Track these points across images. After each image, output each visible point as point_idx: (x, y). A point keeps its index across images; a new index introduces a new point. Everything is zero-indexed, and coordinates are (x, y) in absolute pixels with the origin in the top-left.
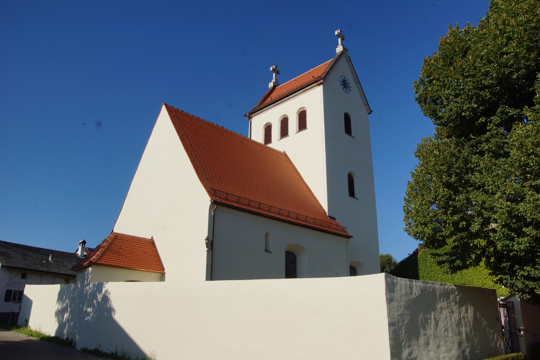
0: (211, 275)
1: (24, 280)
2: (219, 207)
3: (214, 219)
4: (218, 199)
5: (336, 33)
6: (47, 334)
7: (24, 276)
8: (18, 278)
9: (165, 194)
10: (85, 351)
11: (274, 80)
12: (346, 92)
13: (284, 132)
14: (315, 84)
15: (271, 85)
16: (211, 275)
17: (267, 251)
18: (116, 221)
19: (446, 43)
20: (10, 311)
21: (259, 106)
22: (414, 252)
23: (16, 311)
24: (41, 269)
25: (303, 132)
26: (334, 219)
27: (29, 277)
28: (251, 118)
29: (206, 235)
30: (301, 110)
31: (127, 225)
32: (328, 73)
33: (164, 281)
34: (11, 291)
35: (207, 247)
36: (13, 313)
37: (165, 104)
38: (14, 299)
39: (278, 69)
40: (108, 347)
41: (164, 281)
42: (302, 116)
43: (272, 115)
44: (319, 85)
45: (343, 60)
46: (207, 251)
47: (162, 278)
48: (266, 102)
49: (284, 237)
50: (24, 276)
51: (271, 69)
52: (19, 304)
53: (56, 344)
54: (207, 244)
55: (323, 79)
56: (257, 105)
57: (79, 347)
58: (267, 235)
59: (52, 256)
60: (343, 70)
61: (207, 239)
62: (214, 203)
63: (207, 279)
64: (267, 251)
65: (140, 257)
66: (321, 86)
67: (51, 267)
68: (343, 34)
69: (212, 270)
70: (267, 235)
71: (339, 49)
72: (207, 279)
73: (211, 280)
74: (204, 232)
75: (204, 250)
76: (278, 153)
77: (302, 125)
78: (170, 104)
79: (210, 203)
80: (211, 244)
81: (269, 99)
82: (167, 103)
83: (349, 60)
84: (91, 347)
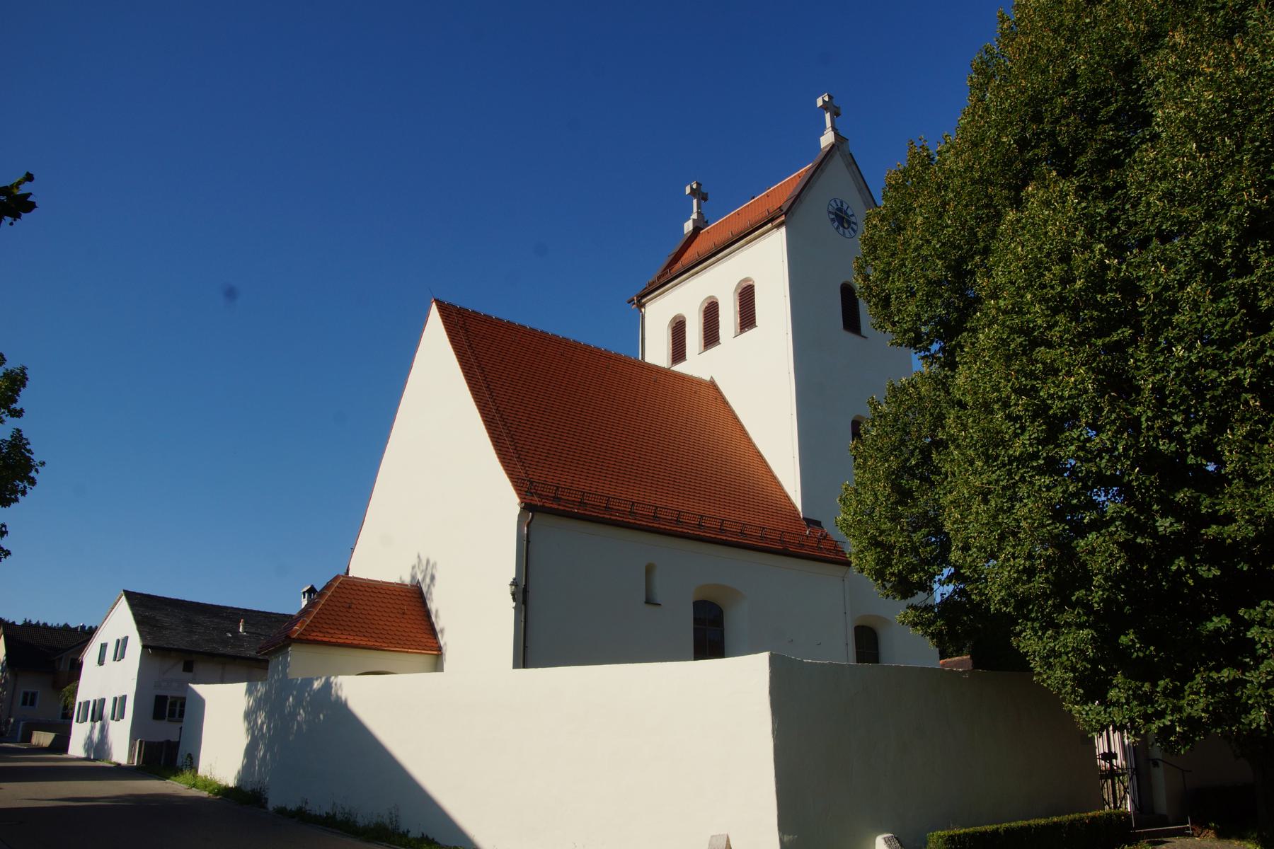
0: (525, 656)
1: (189, 675)
2: (538, 517)
3: (528, 542)
4: (536, 501)
5: (820, 103)
6: (224, 783)
7: (188, 667)
8: (177, 671)
9: (440, 495)
10: (282, 812)
11: (694, 216)
12: (844, 235)
13: (711, 337)
14: (770, 225)
15: (688, 227)
16: (525, 656)
17: (649, 601)
18: (353, 549)
19: (890, 186)
20: (162, 740)
21: (659, 278)
22: (439, 649)
23: (174, 738)
24: (222, 650)
25: (714, 350)
26: (818, 523)
27: (199, 668)
28: (643, 305)
29: (511, 573)
30: (744, 285)
31: (377, 559)
32: (797, 199)
33: (442, 670)
34: (166, 697)
35: (514, 599)
36: (168, 742)
37: (437, 301)
38: (172, 714)
39: (703, 190)
40: (368, 810)
41: (442, 670)
42: (746, 296)
43: (684, 299)
44: (779, 226)
45: (838, 162)
46: (515, 608)
47: (437, 666)
48: (675, 269)
49: (689, 571)
50: (188, 667)
51: (688, 190)
52: (178, 725)
53: (241, 800)
54: (513, 594)
55: (786, 214)
56: (659, 272)
57: (273, 802)
58: (649, 570)
59: (245, 623)
60: (838, 185)
61: (515, 583)
62: (527, 507)
63: (516, 666)
64: (649, 601)
65: (398, 622)
66: (783, 230)
67: (242, 646)
68: (835, 102)
69: (525, 647)
70: (649, 570)
71: (827, 139)
72: (516, 666)
73: (524, 667)
74: (507, 568)
75: (507, 608)
76: (697, 382)
77: (747, 319)
78: (447, 299)
79: (518, 509)
80: (522, 592)
81: (678, 266)
82: (441, 299)
83: (852, 162)
84: (292, 806)
